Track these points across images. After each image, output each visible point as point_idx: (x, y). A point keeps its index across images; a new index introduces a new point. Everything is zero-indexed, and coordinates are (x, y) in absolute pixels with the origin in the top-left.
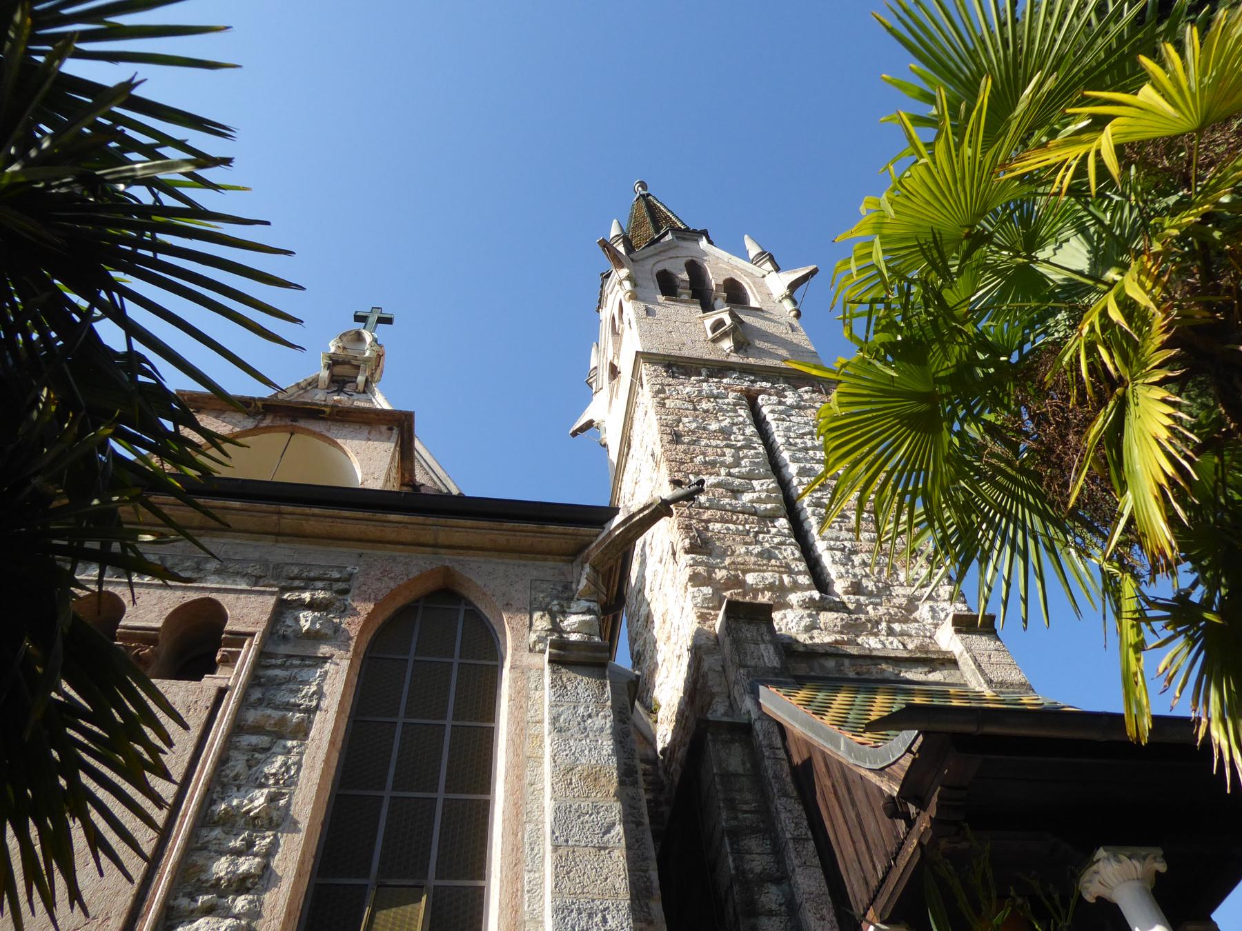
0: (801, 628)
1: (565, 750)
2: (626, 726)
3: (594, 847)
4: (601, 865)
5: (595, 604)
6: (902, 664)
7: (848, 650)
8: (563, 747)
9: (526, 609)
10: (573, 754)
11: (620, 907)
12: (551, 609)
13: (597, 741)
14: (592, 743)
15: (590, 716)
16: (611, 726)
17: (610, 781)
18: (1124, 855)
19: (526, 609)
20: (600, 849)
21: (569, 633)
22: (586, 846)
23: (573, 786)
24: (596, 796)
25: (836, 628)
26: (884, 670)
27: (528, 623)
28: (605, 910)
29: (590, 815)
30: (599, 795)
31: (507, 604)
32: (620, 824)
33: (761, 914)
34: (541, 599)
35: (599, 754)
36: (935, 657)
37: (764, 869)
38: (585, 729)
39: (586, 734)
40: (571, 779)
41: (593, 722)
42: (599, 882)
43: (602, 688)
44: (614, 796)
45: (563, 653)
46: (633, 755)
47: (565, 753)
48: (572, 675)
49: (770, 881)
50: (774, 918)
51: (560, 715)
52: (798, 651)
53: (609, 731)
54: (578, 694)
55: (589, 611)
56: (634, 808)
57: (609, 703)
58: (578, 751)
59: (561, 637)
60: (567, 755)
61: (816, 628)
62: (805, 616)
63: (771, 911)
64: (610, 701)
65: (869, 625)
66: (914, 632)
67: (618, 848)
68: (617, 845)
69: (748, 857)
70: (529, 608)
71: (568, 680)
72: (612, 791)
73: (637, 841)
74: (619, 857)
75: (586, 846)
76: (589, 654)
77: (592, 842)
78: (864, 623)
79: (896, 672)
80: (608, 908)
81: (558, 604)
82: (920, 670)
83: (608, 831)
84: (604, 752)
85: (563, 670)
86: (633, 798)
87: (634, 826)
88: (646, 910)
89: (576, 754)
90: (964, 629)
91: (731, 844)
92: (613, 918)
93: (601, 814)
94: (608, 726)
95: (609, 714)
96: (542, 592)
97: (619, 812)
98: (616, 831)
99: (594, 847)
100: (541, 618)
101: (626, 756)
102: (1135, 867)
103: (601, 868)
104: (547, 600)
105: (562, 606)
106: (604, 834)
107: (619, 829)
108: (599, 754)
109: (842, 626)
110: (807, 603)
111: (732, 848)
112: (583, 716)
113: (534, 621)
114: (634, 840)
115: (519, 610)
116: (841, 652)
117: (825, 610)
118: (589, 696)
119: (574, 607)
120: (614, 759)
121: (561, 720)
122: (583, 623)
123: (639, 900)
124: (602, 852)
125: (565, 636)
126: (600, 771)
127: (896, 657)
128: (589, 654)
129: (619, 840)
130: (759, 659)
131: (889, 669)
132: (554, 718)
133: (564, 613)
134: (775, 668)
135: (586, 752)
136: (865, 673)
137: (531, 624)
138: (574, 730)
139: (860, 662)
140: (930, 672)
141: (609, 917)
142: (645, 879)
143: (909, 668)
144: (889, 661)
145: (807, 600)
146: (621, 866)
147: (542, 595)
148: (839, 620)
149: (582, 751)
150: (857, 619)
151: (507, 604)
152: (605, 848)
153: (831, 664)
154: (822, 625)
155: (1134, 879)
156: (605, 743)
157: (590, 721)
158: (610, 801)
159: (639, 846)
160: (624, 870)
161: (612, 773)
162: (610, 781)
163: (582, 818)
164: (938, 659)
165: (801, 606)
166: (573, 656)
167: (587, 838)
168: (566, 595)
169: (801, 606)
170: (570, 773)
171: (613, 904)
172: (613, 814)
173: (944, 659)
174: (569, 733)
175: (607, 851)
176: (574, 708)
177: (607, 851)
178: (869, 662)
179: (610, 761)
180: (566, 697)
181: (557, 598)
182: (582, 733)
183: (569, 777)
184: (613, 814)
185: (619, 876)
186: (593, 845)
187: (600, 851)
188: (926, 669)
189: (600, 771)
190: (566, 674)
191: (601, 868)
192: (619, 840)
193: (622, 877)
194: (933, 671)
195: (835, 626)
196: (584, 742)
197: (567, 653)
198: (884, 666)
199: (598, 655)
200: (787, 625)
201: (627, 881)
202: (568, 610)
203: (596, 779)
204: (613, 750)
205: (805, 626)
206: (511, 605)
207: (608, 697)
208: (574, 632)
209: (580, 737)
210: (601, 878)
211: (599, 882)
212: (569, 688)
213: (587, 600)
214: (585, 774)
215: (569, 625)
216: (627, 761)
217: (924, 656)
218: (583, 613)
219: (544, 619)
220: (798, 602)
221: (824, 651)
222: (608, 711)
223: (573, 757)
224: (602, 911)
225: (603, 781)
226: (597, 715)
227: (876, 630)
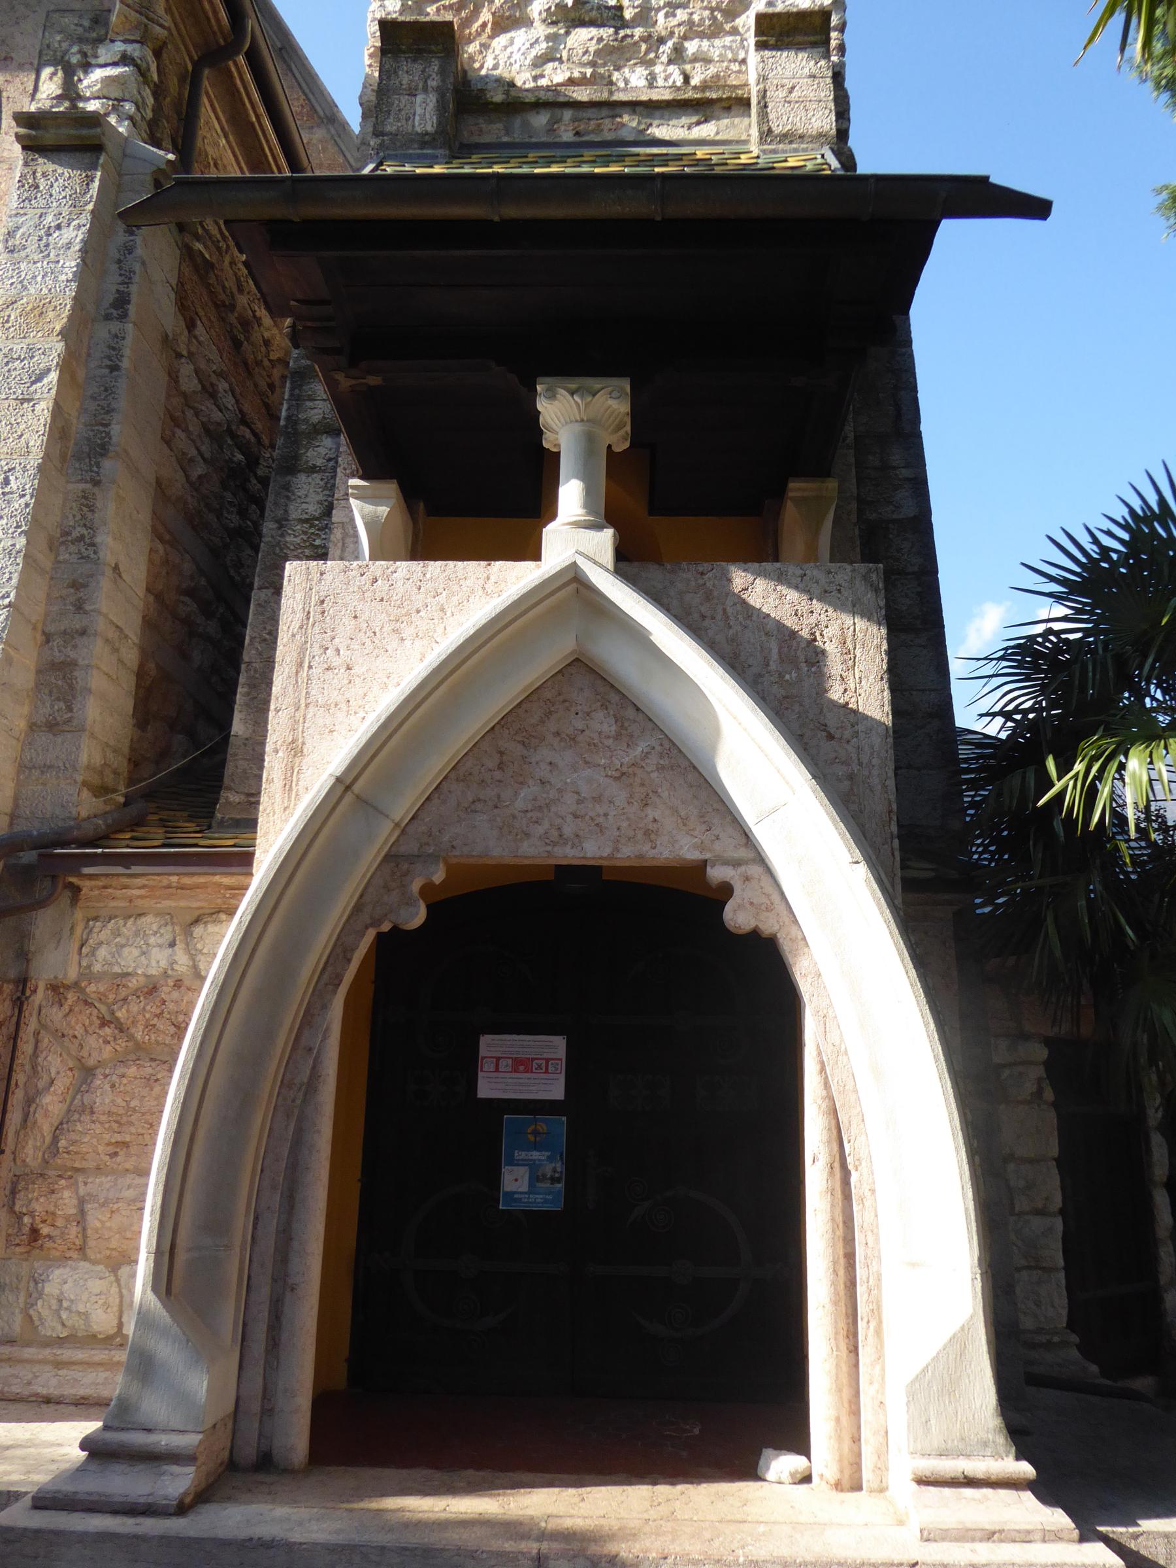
0: (527, 62)
1: (12, 277)
2: (132, 238)
3: (16, 399)
4: (19, 420)
5: (137, 46)
6: (658, 113)
7: (575, 95)
8: (10, 272)
9: (31, 64)
10: (21, 282)
11: (28, 467)
12: (68, 62)
13: (58, 262)
14: (51, 265)
15: (59, 227)
16: (82, 240)
17: (59, 315)
18: (564, 389)
19: (31, 64)
20: (23, 401)
21: (89, 99)
22: (7, 399)
23: (10, 324)
24: (36, 338)
25: (586, 57)
26: (623, 125)
27: (32, 88)
28: (10, 470)
29: (22, 361)
30: (40, 334)
31: (6, 59)
32: (55, 371)
33: (300, 471)
34: (56, 45)
35: (56, 279)
36: (714, 96)
37: (324, 418)
38: (47, 245)
39: (46, 253)
40: (9, 316)
41: (61, 235)
42: (11, 440)
43: (88, 184)
44: (57, 335)
45: (34, 133)
46: (130, 278)
47: (11, 281)
48: (50, 167)
49: (326, 433)
50: (315, 475)
51: (18, 228)
52: (492, 103)
53: (77, 248)
54: (51, 195)
55: (124, 60)
56: (114, 349)
57: (90, 207)
58: (28, 277)
59: (75, 107)
60: (12, 284)
61: (553, 60)
62: (542, 38)
63: (315, 466)
64: (92, 204)
65: (644, 47)
66: (717, 53)
67: (44, 399)
68: (45, 396)
69: (309, 404)
70: (36, 62)
71: (44, 175)
72: (58, 328)
73: (106, 390)
74: (43, 410)
75: (7, 399)
76: (73, 132)
77: (14, 393)
78: (636, 43)
79: (642, 127)
80: (14, 468)
81: (80, 52)
82: (684, 120)
83: (39, 379)
84: (64, 278)
85: (41, 160)
86: (116, 336)
87: (107, 371)
88: (95, 469)
89: (25, 282)
90: (772, 41)
91: (292, 389)
92: (16, 478)
93: (36, 359)
94: (78, 240)
95: (84, 222)
96: (60, 32)
97: (59, 355)
98: (50, 380)
99: (16, 399)
100: (51, 78)
101: (120, 279)
102: (576, 402)
103: (18, 423)
104: (65, 45)
105: (85, 55)
106: (33, 383)
107: (54, 376)
108: (56, 279)
109: (598, 53)
110: (554, 14)
111: (291, 395)
112: (49, 228)
113: (41, 84)
114: (103, 388)
115: (21, 67)
116: (561, 99)
117: (583, 24)
118: (65, 197)
119: (105, 53)
120: (74, 285)
121: (18, 236)
122: (107, 81)
123: (90, 458)
124: (25, 405)
125: (81, 105)
126: (50, 302)
127: (650, 101)
128: (73, 132)
129: (49, 389)
130: (407, 119)
131: (630, 121)
132: (9, 232)
133: (87, 67)
134: (427, 134)
135: (39, 279)
136: (589, 133)
137: (36, 89)
138: (32, 247)
139: (590, 113)
140: (698, 123)
141: (12, 478)
142: (104, 435)
143: (665, 119)
144: (638, 109)
145: (553, 8)
146: (42, 421)
147: (58, 38)
148: (594, 41)
149: (34, 277)
150: (626, 36)
151: (6, 59)
152: (29, 400)
153: (541, 120)
154: (565, 55)
155: (577, 421)
156: (67, 264)
157: (57, 233)
158: (52, 341)
159: (106, 396)
160: (45, 425)
161: (66, 305)
162: (59, 315)
163: (11, 365)
164: (720, 100)
165: (544, 21)
166: (49, 137)
167: (10, 389)
168: (94, 35)
169: (544, 21)
170: (11, 307)
171: (20, 464)
172: (51, 358)
173: (729, 98)
174: (23, 254)
175: (31, 404)
176: (41, 217)
177: (31, 404)
178: (605, 112)
179: (67, 289)
180: (33, 202)
181: (81, 40)
182: (42, 252)
183: (7, 313)
184: (51, 358)
185: (37, 432)
186: (15, 397)
187: (22, 404)
188: (694, 119)
189: (50, 302)
190: (44, 165)
191: (18, 423)
192: (49, 389)
193: (41, 433)
194: (706, 121)
195: (586, 52)
196: (39, 265)
197: (40, 132)
198: (626, 118)
199: (85, 132)
200: (509, 58)
201: (45, 438)
202: (93, 61)
203: (42, 313)
204: (75, 274)
205: (536, 57)
206: (12, 59)
207: (91, 197)
208: (95, 98)
209: (36, 259)
210: (15, 435)
211: (11, 440)
212: (41, 188)
213: (125, 41)
214: (29, 308)
215: (89, 87)
216: (121, 288)
217: (698, 96)
218: (115, 64)
219: (55, 79)
220: (540, 13)
221: (533, 100)
222: (85, 219)
223: (19, 286)
224: (5, 473)
225: (51, 314)
226: (69, 225)
227: (652, 55)
